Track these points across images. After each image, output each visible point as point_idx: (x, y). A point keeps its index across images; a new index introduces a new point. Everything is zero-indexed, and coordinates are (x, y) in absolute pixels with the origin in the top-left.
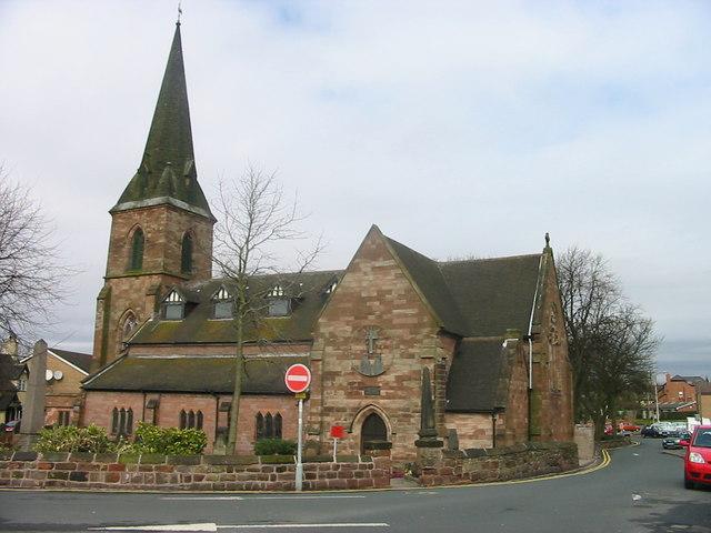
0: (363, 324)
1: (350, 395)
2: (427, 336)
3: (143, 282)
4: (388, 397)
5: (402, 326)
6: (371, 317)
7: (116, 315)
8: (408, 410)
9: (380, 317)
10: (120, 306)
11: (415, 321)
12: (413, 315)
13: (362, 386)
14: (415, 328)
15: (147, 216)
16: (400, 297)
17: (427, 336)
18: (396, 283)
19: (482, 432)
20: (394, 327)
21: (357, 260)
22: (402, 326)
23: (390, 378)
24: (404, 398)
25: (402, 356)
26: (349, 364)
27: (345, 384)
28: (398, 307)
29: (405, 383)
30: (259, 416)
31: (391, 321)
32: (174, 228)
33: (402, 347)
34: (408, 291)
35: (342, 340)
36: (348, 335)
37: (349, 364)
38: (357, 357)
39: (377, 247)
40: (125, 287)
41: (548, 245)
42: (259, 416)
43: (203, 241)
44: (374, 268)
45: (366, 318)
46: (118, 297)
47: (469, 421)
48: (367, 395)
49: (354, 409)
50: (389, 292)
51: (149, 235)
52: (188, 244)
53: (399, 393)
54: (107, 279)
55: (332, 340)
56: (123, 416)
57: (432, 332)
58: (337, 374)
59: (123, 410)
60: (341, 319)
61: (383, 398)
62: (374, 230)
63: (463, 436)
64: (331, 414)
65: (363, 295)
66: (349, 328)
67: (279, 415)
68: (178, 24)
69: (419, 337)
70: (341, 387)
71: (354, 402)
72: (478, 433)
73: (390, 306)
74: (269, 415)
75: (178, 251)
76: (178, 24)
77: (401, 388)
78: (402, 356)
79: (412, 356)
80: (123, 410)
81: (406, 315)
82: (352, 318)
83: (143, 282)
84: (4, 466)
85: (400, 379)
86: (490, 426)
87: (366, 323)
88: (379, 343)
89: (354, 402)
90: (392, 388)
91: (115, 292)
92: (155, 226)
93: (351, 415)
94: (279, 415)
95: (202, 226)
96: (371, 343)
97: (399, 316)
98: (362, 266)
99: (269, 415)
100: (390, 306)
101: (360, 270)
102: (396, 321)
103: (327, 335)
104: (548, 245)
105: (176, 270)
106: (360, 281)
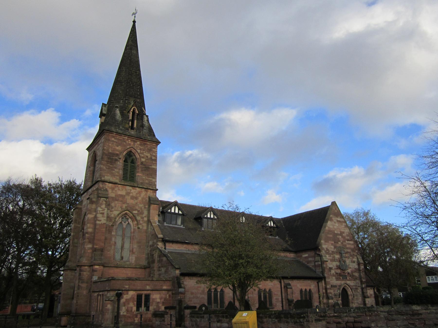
1: (337, 279)
3: (140, 193)
5: (350, 248)
6: (339, 243)
13: (340, 275)
15: (140, 145)
16: (347, 235)
27: (335, 274)
30: (301, 290)
31: (346, 245)
35: (331, 252)
36: (333, 250)
39: (88, 149)
40: (123, 193)
42: (301, 290)
44: (337, 221)
45: (338, 243)
48: (343, 279)
51: (143, 160)
56: (216, 295)
61: (348, 280)
65: (336, 232)
66: (333, 247)
67: (310, 290)
68: (134, 22)
70: (333, 275)
71: (339, 283)
74: (306, 290)
76: (134, 22)
82: (333, 242)
83: (140, 193)
84: (436, 313)
89: (339, 283)
94: (310, 290)
98: (333, 218)
99: (306, 290)
101: (333, 220)
103: (325, 249)
106: (334, 226)
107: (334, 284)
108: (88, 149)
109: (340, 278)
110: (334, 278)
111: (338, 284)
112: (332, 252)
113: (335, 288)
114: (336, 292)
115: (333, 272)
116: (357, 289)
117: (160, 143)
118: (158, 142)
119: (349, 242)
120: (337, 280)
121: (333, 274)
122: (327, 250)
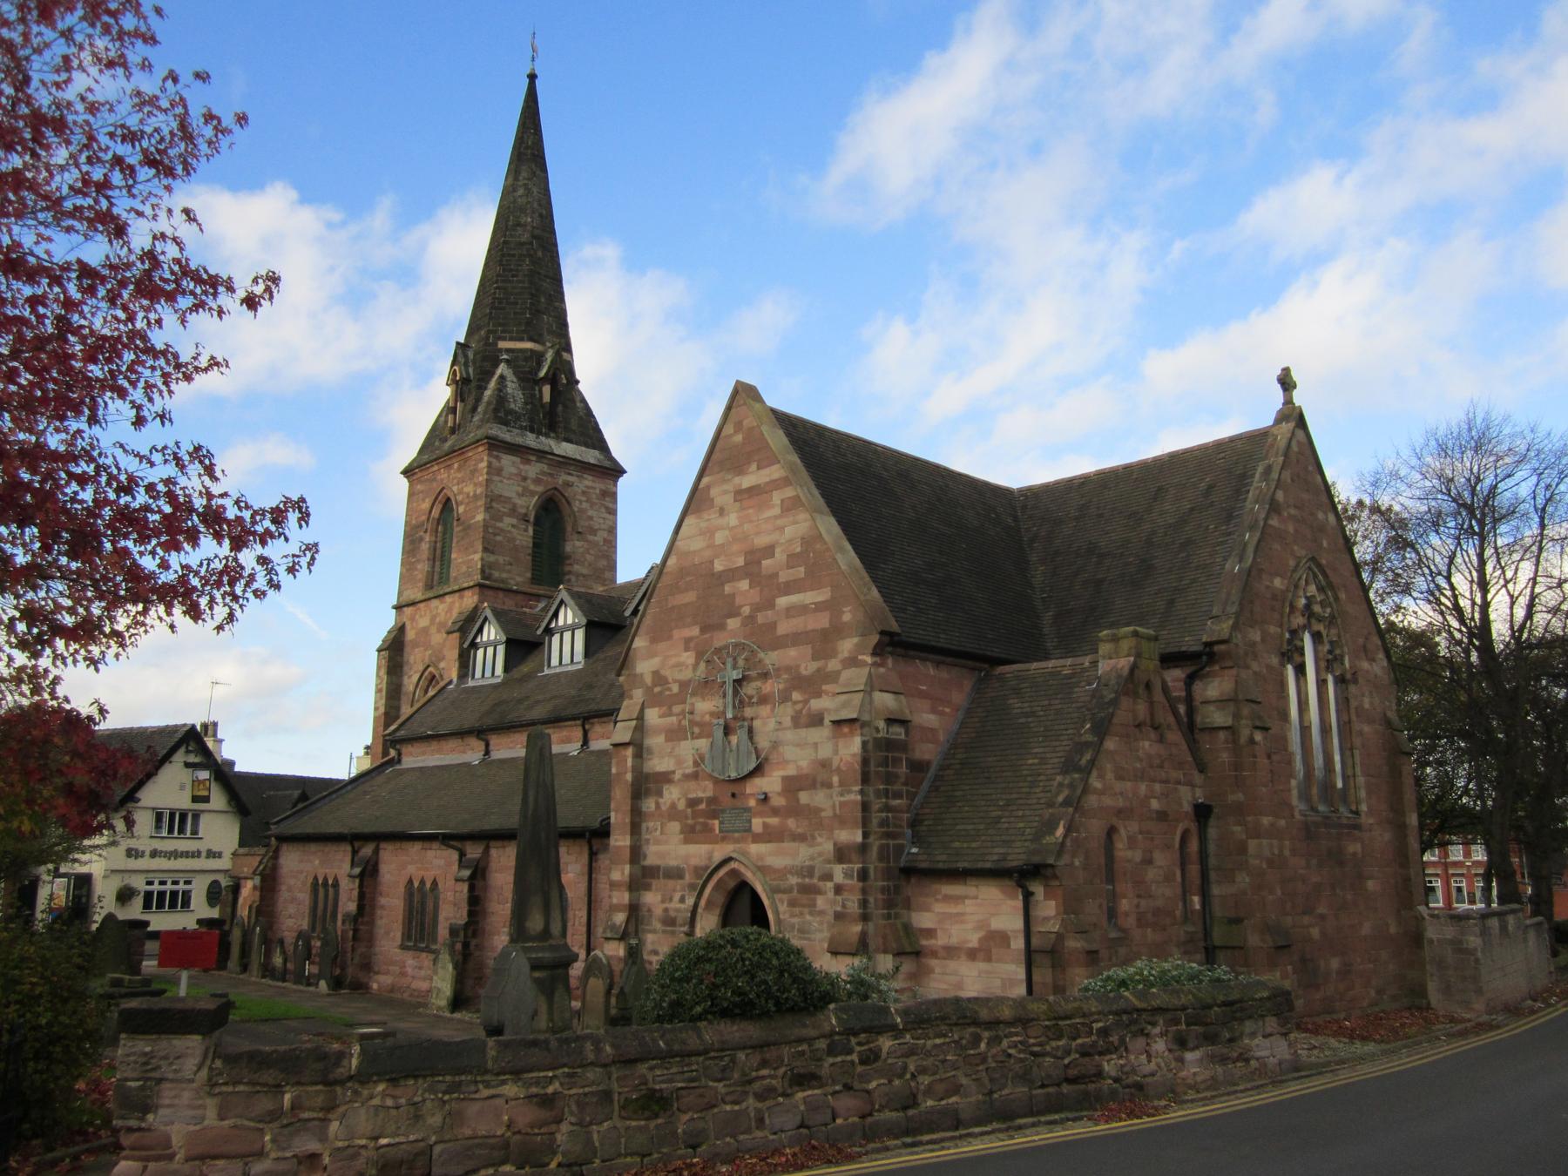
0: (718, 644)
1: (691, 834)
2: (852, 662)
4: (769, 836)
5: (795, 639)
6: (733, 623)
7: (410, 681)
8: (810, 871)
9: (751, 618)
10: (416, 660)
11: (822, 621)
12: (820, 607)
14: (823, 642)
17: (852, 662)
18: (793, 523)
19: (1002, 938)
20: (779, 643)
21: (705, 480)
22: (795, 639)
23: (770, 783)
24: (801, 838)
25: (797, 722)
26: (688, 749)
27: (681, 805)
28: (789, 588)
29: (804, 797)
31: (772, 626)
32: (509, 489)
33: (796, 696)
34: (809, 541)
35: (675, 689)
36: (687, 674)
37: (688, 749)
38: (704, 730)
39: (407, 472)
41: (1288, 401)
43: (597, 516)
44: (741, 495)
46: (415, 644)
47: (969, 907)
49: (697, 871)
50: (769, 551)
52: (551, 518)
53: (791, 823)
54: (398, 608)
55: (659, 693)
57: (859, 649)
58: (666, 778)
59: (326, 879)
60: (677, 634)
61: (757, 839)
62: (743, 395)
63: (951, 952)
64: (654, 882)
66: (688, 658)
68: (532, 77)
69: (833, 665)
70: (673, 813)
72: (993, 942)
73: (771, 587)
75: (524, 537)
76: (532, 77)
77: (795, 810)
78: (797, 722)
79: (816, 720)
80: (326, 879)
81: (803, 609)
85: (793, 785)
86: (1019, 924)
87: (720, 639)
88: (749, 689)
90: (775, 812)
91: (410, 635)
92: (469, 489)
93: (692, 887)
95: (583, 485)
96: (730, 692)
97: (790, 612)
100: (771, 587)
102: (783, 628)
104: (1288, 401)
105: (519, 577)
107: (673, 863)
108: (407, 472)
109: (707, 829)
110: (675, 827)
111: (695, 862)
112: (684, 685)
113: (671, 883)
114: (675, 904)
115: (672, 795)
116: (810, 891)
117: (743, 395)
118: (617, 471)
119: (794, 599)
120: (687, 841)
121: (673, 806)
122: (659, 678)
